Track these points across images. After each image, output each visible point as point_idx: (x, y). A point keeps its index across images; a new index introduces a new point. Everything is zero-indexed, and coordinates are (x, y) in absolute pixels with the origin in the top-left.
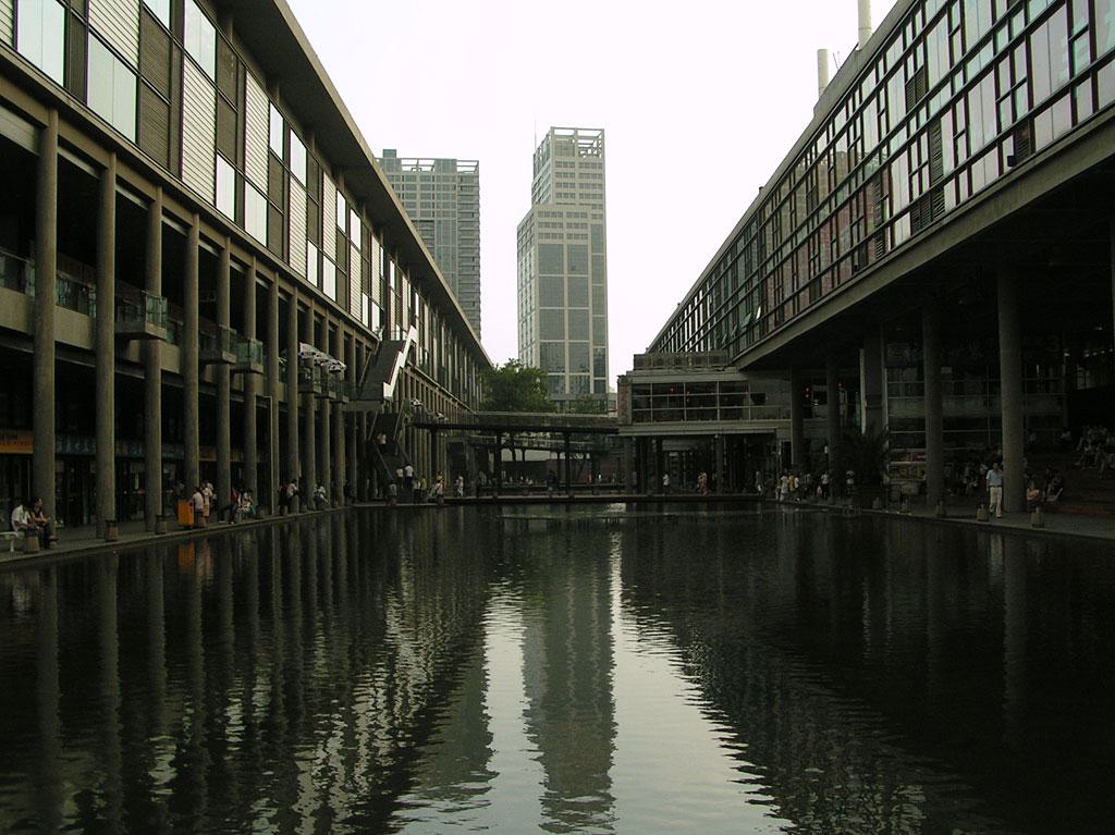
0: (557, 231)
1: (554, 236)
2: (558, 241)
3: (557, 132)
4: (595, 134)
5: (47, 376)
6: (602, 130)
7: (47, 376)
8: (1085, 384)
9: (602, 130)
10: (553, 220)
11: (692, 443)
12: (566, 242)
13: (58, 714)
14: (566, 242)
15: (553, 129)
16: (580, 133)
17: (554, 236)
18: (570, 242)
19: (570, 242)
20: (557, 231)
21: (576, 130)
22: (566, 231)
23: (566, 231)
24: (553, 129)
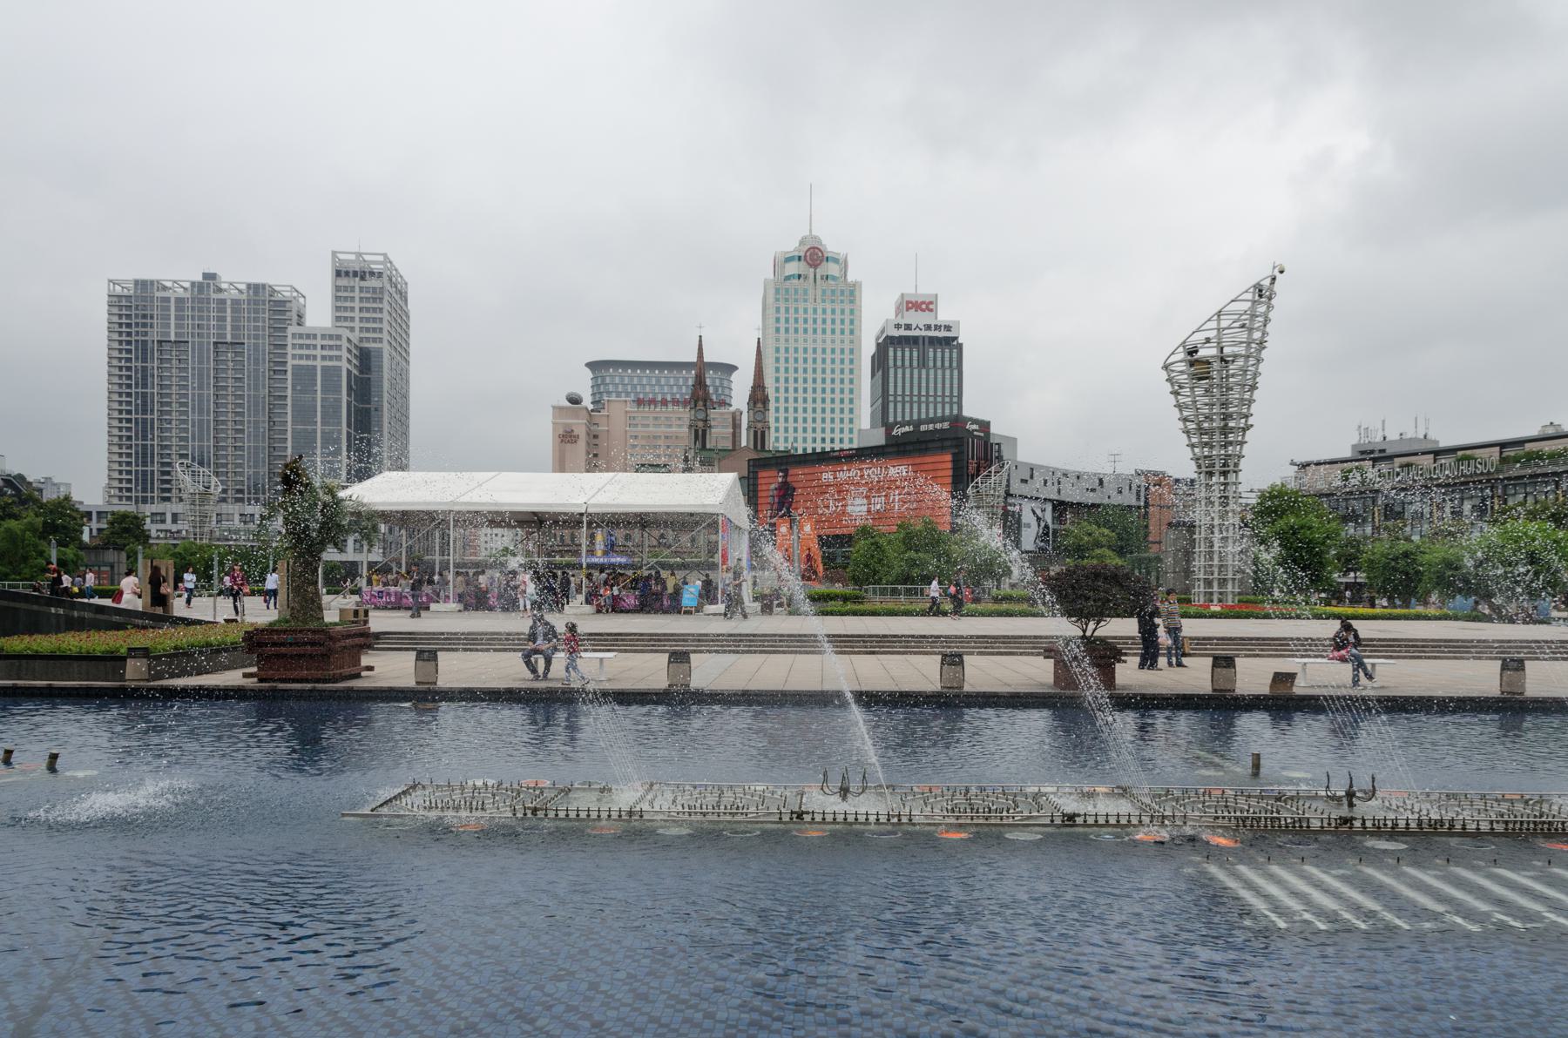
1: (308, 357)
3: (341, 256)
4: (381, 258)
14: (319, 363)
15: (334, 253)
16: (367, 258)
17: (308, 357)
18: (296, 362)
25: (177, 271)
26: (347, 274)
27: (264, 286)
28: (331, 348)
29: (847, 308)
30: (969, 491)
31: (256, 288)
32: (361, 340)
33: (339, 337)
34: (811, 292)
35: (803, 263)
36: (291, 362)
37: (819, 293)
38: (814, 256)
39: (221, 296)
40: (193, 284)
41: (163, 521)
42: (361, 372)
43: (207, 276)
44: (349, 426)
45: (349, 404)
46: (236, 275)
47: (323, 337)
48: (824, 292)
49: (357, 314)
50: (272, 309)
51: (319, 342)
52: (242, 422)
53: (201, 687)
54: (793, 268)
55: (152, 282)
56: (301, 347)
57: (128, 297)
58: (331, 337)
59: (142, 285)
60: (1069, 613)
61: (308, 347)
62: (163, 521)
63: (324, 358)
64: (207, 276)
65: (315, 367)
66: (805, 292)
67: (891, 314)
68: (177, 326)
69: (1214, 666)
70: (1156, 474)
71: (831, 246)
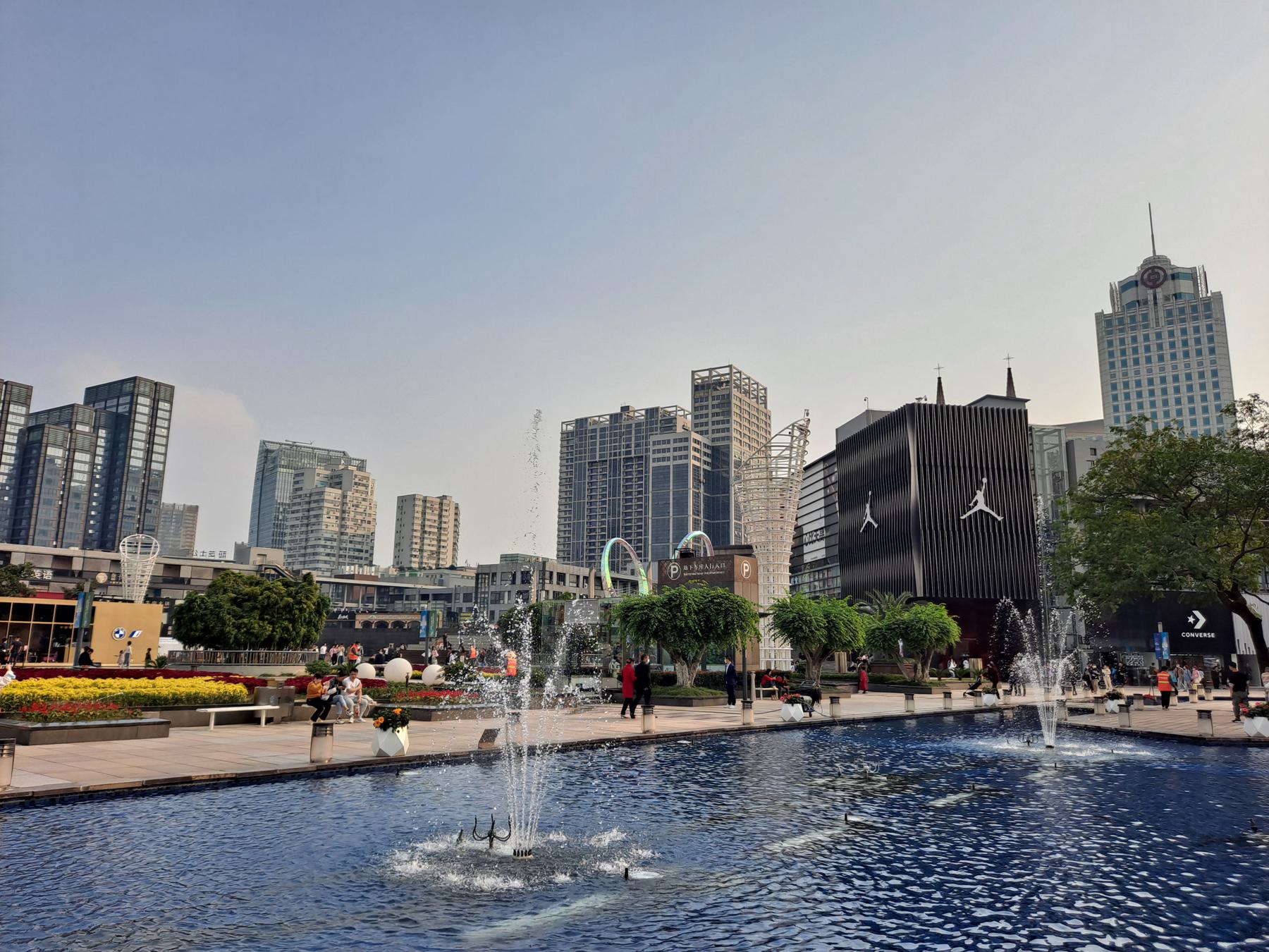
4: (727, 370)
12: (671, 463)
14: (671, 463)
15: (693, 373)
17: (664, 459)
18: (656, 464)
25: (600, 407)
27: (657, 409)
29: (1202, 324)
32: (713, 440)
34: (1152, 316)
35: (1141, 287)
36: (652, 465)
37: (1161, 314)
38: (1156, 273)
39: (630, 422)
42: (713, 465)
44: (697, 512)
45: (696, 496)
46: (640, 404)
48: (1169, 313)
53: (137, 696)
54: (1130, 296)
56: (659, 451)
57: (572, 433)
59: (581, 422)
60: (180, 639)
61: (664, 451)
65: (686, 466)
66: (1145, 317)
69: (314, 735)
70: (329, 459)
71: (1180, 260)
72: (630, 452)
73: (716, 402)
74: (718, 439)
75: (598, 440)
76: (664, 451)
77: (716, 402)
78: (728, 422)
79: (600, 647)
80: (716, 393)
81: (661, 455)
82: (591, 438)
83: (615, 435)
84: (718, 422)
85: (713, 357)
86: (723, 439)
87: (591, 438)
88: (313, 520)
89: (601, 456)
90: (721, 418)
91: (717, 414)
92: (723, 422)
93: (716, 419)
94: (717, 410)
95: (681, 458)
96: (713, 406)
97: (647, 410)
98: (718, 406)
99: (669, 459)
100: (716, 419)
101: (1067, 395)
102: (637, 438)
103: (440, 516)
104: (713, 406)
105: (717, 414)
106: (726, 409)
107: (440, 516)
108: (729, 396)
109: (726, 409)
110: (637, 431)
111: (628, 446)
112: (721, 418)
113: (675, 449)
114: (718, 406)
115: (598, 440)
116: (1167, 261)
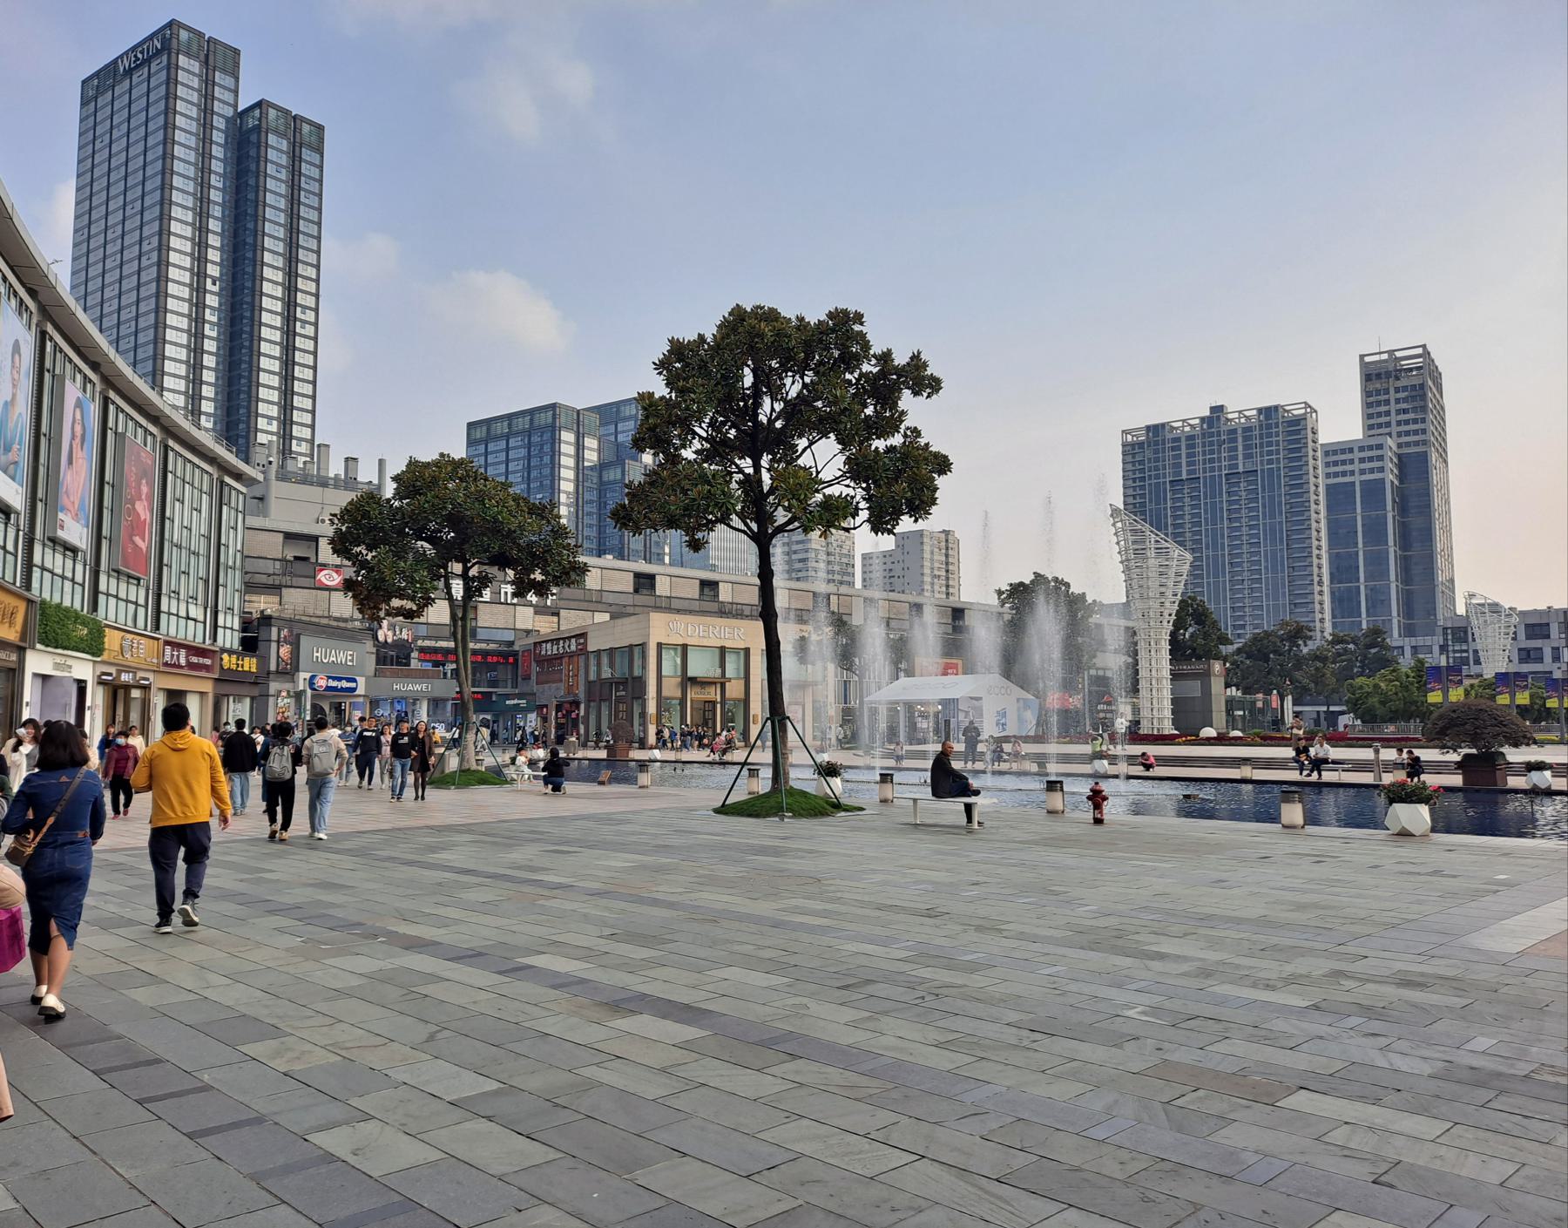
0: (1348, 468)
1: (1344, 474)
2: (1348, 479)
3: (1367, 359)
4: (1420, 351)
5: (1318, 482)
6: (1424, 346)
7: (1318, 482)
8: (270, 418)
9: (1424, 346)
10: (1343, 457)
11: (363, 981)
12: (1357, 479)
13: (824, 534)
14: (1357, 479)
15: (1362, 357)
16: (1398, 354)
17: (1344, 474)
18: (1364, 477)
19: (1364, 477)
20: (1348, 468)
21: (1391, 352)
22: (1356, 467)
23: (1356, 467)
24: (1362, 357)
25: (1182, 407)
26: (1379, 376)
28: (1371, 459)
30: (575, 1020)
31: (1268, 412)
33: (1380, 447)
40: (1203, 419)
41: (1540, 660)
42: (1401, 482)
43: (1213, 409)
46: (1244, 400)
47: (1362, 449)
49: (1394, 418)
50: (1283, 430)
51: (1357, 455)
52: (1259, 581)
55: (1163, 425)
57: (1141, 444)
58: (1370, 448)
59: (1155, 430)
61: (1344, 462)
62: (1540, 660)
63: (1362, 472)
64: (1213, 409)
65: (1383, 480)
67: (15, 485)
68: (1189, 464)
72: (1236, 466)
73: (1402, 395)
74: (1408, 444)
75: (1184, 452)
76: (1344, 462)
77: (1402, 395)
78: (1423, 420)
79: (442, 750)
80: (1399, 384)
81: (1340, 469)
82: (1173, 449)
83: (1211, 444)
84: (1407, 422)
85: (1394, 336)
86: (1417, 443)
87: (1173, 449)
88: (798, 566)
89: (1189, 473)
90: (1411, 416)
91: (1405, 411)
92: (1415, 421)
93: (1402, 417)
94: (1405, 406)
95: (1372, 471)
96: (1398, 401)
97: (1260, 410)
98: (1405, 400)
99: (1352, 473)
100: (1402, 417)
101: (1340, 420)
102: (1246, 447)
103: (947, 556)
104: (1398, 401)
105: (1405, 411)
106: (1419, 403)
107: (947, 556)
108: (1422, 386)
109: (1419, 403)
110: (1245, 439)
111: (1232, 458)
112: (1411, 416)
113: (1362, 460)
114: (1405, 400)
115: (1184, 452)
116: (772, 316)
